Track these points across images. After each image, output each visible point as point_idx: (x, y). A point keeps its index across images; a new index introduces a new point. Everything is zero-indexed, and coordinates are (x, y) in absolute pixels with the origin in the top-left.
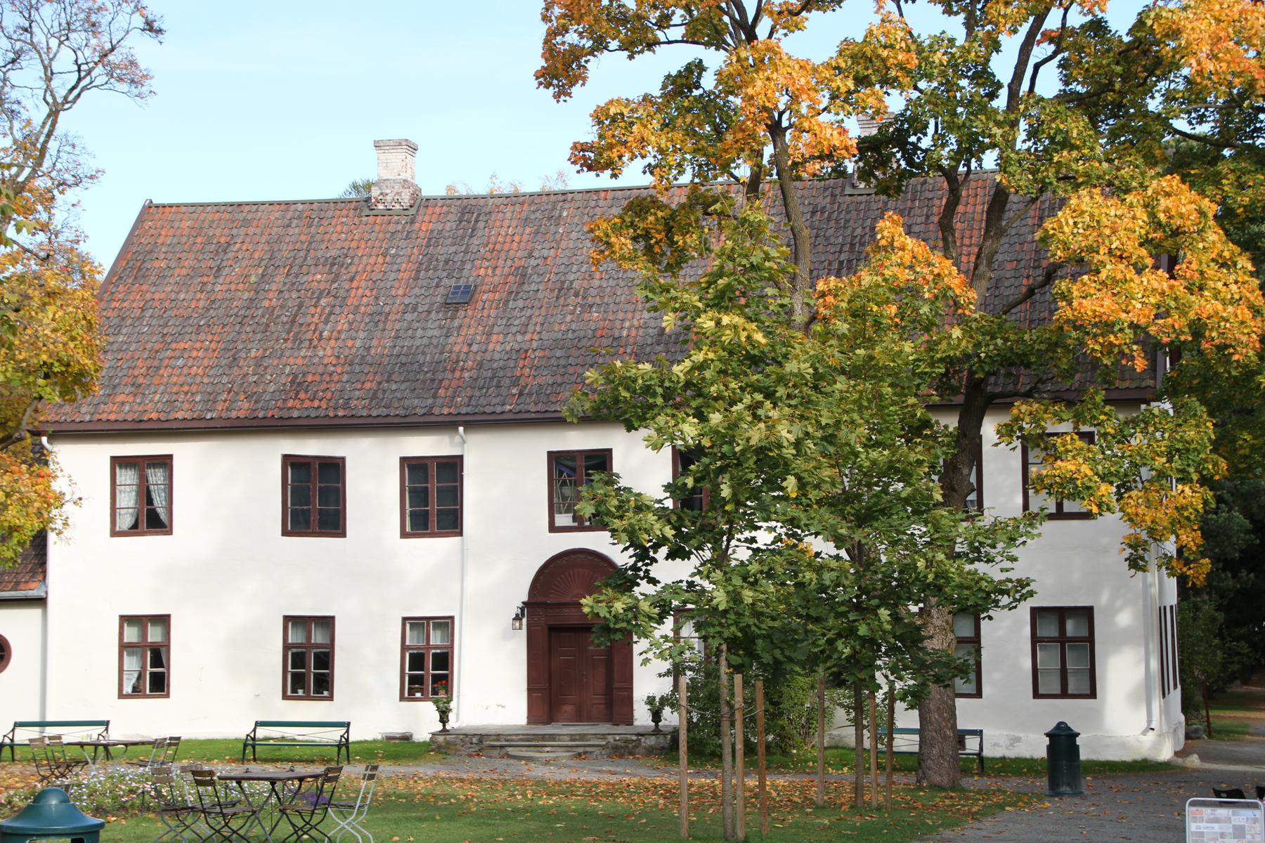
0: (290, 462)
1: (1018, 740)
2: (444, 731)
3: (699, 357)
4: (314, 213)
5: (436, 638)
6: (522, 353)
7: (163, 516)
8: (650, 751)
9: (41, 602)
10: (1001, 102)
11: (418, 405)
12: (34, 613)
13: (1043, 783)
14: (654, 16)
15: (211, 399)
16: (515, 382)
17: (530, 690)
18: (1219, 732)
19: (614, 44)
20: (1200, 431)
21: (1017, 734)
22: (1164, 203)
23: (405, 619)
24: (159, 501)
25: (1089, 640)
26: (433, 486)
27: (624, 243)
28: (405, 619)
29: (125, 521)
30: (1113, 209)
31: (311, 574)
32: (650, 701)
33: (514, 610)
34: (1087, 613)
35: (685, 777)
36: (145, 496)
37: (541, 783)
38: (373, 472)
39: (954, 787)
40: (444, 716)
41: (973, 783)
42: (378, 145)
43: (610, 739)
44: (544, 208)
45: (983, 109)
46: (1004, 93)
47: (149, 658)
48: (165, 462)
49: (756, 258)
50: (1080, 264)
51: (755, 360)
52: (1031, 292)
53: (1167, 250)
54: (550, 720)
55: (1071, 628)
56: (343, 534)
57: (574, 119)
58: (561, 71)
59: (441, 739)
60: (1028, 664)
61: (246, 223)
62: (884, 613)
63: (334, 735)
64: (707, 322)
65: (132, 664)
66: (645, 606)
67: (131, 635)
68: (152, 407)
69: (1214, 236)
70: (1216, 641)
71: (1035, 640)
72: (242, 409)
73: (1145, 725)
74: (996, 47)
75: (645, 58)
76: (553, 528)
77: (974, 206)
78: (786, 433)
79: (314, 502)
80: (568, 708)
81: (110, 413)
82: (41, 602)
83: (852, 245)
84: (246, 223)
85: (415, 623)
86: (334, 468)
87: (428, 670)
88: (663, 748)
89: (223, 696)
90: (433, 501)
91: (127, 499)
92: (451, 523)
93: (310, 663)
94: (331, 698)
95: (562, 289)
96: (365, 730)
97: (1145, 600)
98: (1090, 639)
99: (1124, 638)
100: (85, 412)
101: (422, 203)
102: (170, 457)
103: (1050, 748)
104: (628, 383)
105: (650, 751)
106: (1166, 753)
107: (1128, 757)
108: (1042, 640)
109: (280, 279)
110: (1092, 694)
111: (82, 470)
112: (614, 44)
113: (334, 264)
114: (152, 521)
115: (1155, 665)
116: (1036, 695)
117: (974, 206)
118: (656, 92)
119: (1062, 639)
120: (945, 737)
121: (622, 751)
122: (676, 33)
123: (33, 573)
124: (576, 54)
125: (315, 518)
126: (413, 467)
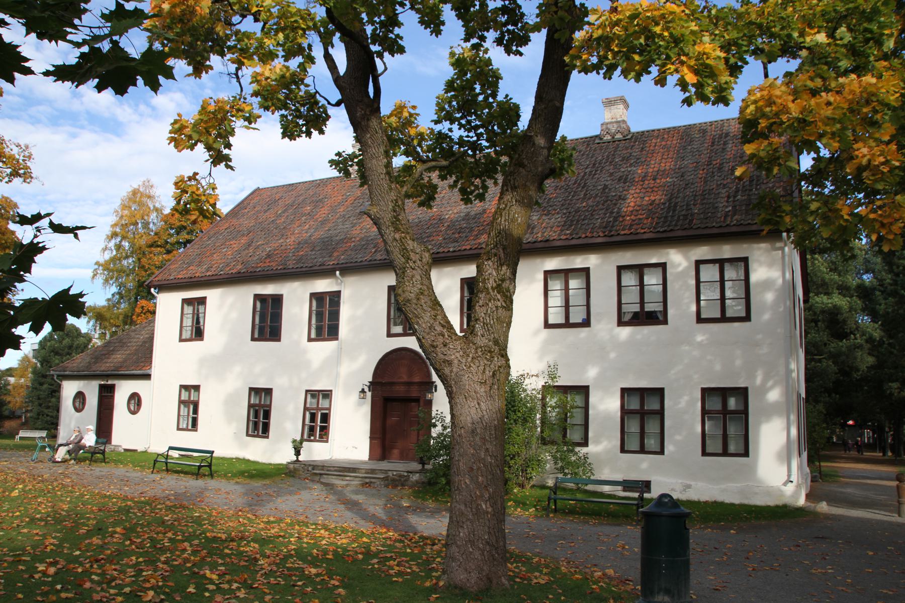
1: (689, 487)
2: (297, 460)
17: (371, 438)
18: (826, 475)
21: (688, 482)
23: (307, 391)
25: (744, 413)
28: (307, 391)
29: (187, 334)
31: (263, 364)
34: (742, 393)
38: (296, 299)
43: (390, 474)
47: (190, 401)
48: (202, 301)
55: (732, 403)
56: (279, 340)
59: (292, 466)
60: (699, 429)
68: (198, 271)
70: (824, 425)
71: (704, 412)
73: (786, 478)
76: (389, 335)
80: (396, 452)
83: (594, 164)
85: (313, 394)
88: (423, 483)
90: (326, 321)
91: (188, 322)
94: (327, 441)
97: (787, 382)
98: (745, 412)
99: (770, 411)
102: (205, 298)
106: (801, 501)
107: (771, 502)
108: (709, 412)
110: (746, 454)
115: (794, 431)
116: (704, 453)
119: (725, 411)
120: (478, 512)
126: (317, 297)
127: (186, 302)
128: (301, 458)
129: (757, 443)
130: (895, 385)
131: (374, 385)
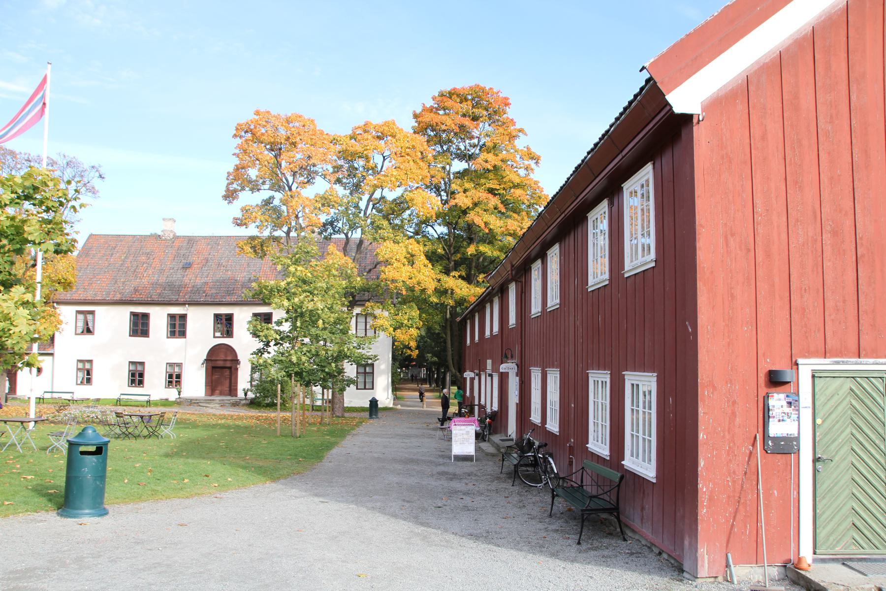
0: (134, 314)
3: (289, 280)
4: (142, 239)
5: (177, 369)
6: (206, 283)
7: (91, 328)
8: (244, 405)
10: (362, 215)
11: (174, 298)
12: (50, 358)
13: (367, 414)
14: (261, 181)
15: (108, 294)
16: (204, 292)
19: (247, 189)
20: (415, 313)
22: (410, 247)
26: (177, 323)
27: (248, 249)
30: (396, 247)
32: (244, 390)
35: (254, 412)
37: (209, 415)
38: (159, 317)
39: (343, 416)
40: (179, 393)
41: (347, 415)
42: (164, 220)
44: (214, 241)
45: (358, 216)
46: (363, 212)
49: (309, 249)
50: (387, 263)
51: (304, 282)
53: (411, 260)
54: (212, 394)
55: (368, 369)
57: (235, 209)
58: (230, 196)
61: (121, 241)
62: (333, 365)
63: (146, 398)
64: (292, 269)
65: (80, 375)
66: (269, 361)
67: (81, 366)
68: (90, 295)
69: (423, 257)
72: (118, 297)
74: (361, 199)
75: (256, 194)
76: (214, 337)
77: (353, 246)
78: (320, 305)
79: (140, 326)
81: (76, 297)
82: (52, 354)
84: (121, 241)
86: (146, 316)
87: (174, 379)
89: (110, 385)
90: (178, 327)
91: (81, 324)
92: (183, 334)
93: (137, 377)
95: (219, 265)
96: (155, 397)
98: (373, 373)
100: (68, 296)
101: (176, 238)
103: (370, 405)
104: (266, 287)
105: (244, 405)
106: (391, 406)
109: (131, 258)
111: (67, 314)
112: (247, 189)
113: (148, 254)
114: (88, 331)
117: (353, 246)
118: (260, 203)
119: (365, 373)
121: (235, 405)
122: (267, 186)
123: (50, 345)
124: (235, 191)
125: (139, 331)
126: (172, 317)
127: (78, 312)
128: (182, 396)
129: (605, 561)
130: (429, 355)
131: (207, 360)
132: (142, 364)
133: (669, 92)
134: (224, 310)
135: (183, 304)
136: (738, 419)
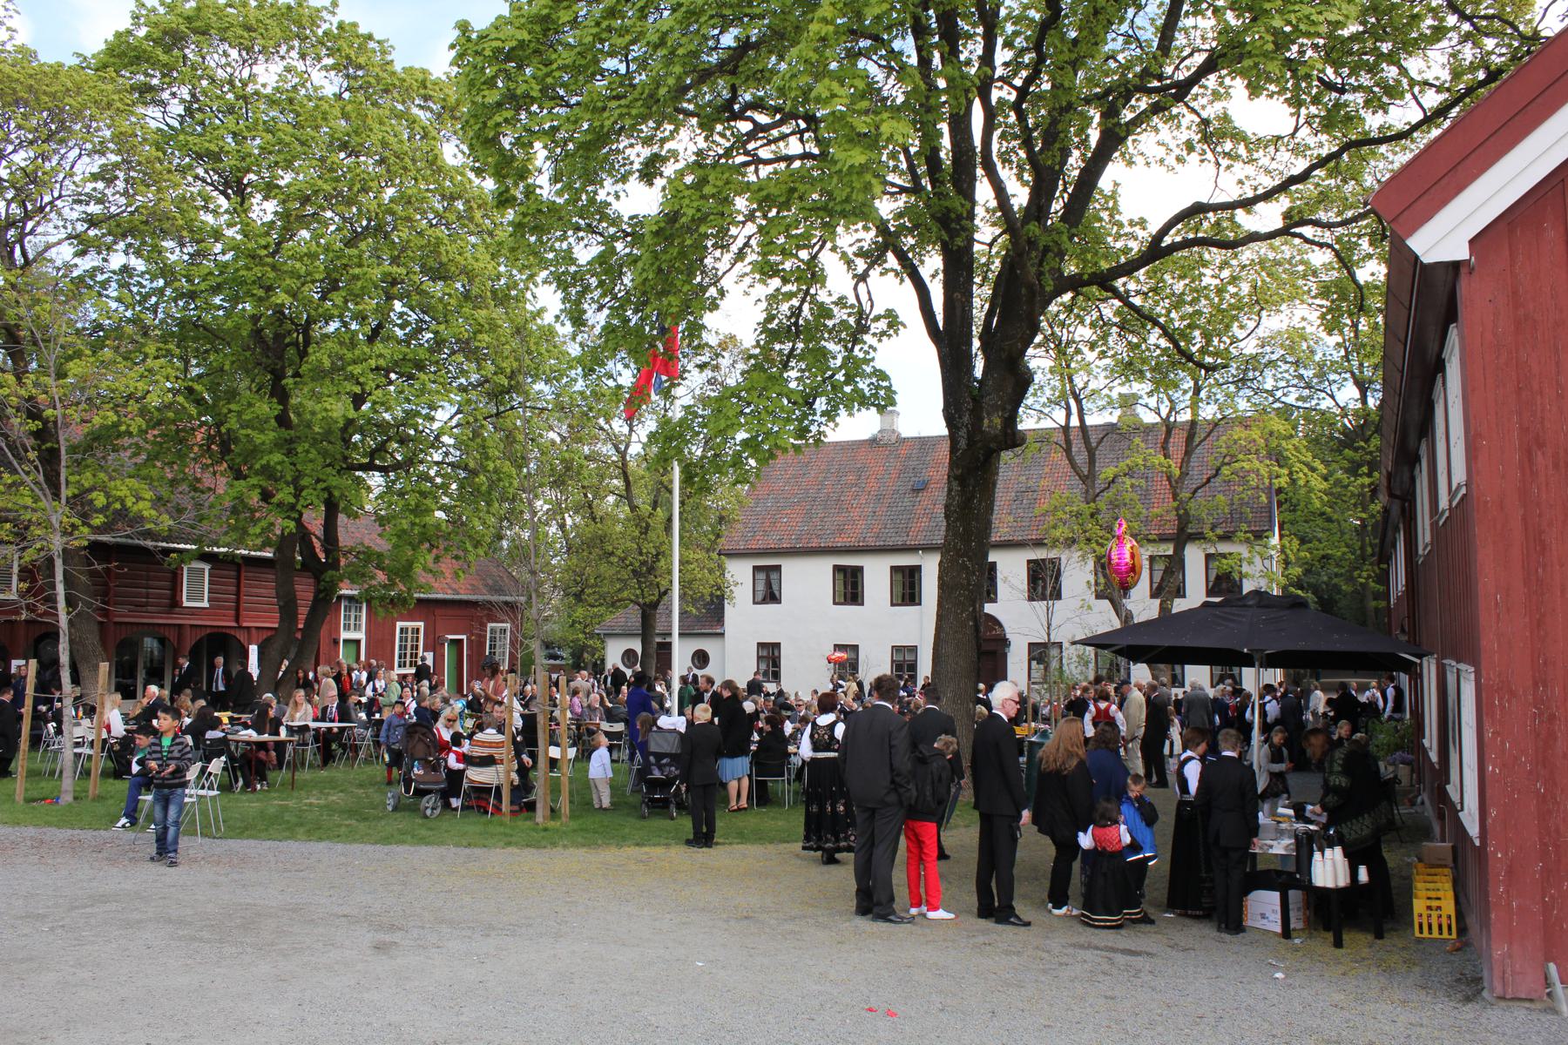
0: (837, 569)
9: (722, 635)
24: (775, 587)
33: (882, 926)
36: (769, 585)
38: (877, 575)
52: (1208, 480)
68: (772, 542)
79: (850, 588)
86: (860, 569)
91: (761, 587)
127: (756, 569)
132: (855, 648)
133: (1410, 234)
134: (1039, 554)
135: (912, 549)
136: (1559, 743)
